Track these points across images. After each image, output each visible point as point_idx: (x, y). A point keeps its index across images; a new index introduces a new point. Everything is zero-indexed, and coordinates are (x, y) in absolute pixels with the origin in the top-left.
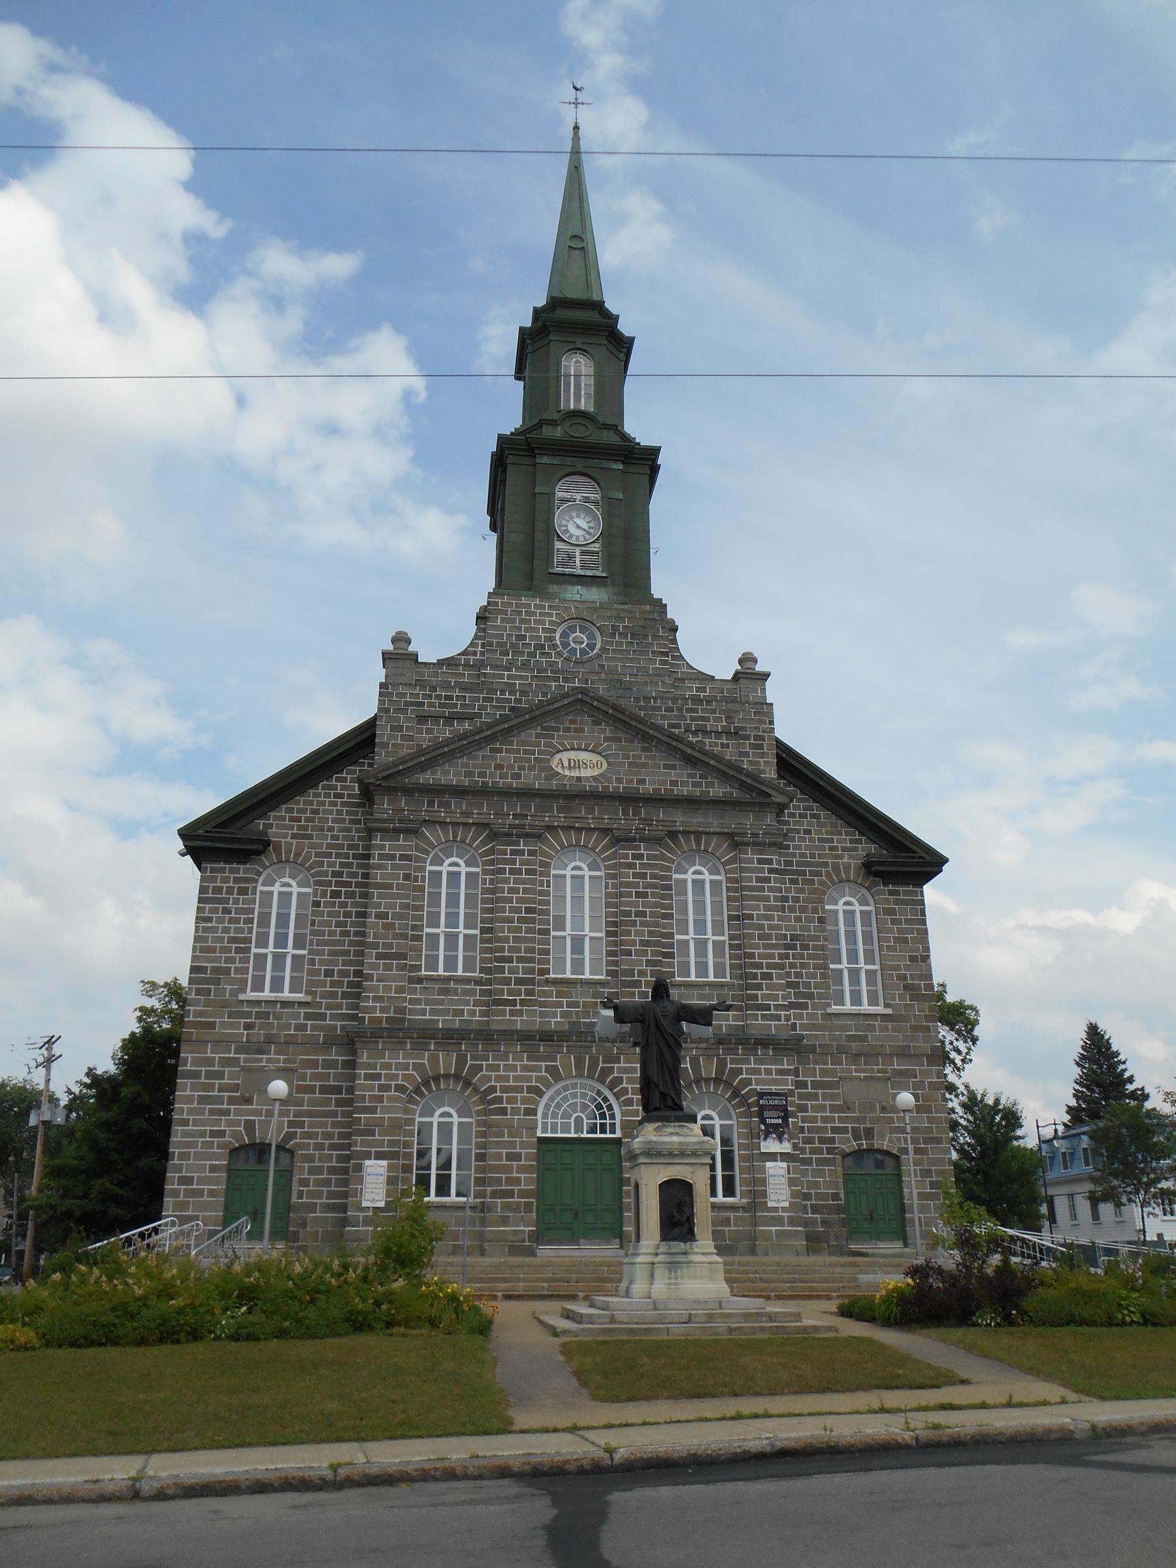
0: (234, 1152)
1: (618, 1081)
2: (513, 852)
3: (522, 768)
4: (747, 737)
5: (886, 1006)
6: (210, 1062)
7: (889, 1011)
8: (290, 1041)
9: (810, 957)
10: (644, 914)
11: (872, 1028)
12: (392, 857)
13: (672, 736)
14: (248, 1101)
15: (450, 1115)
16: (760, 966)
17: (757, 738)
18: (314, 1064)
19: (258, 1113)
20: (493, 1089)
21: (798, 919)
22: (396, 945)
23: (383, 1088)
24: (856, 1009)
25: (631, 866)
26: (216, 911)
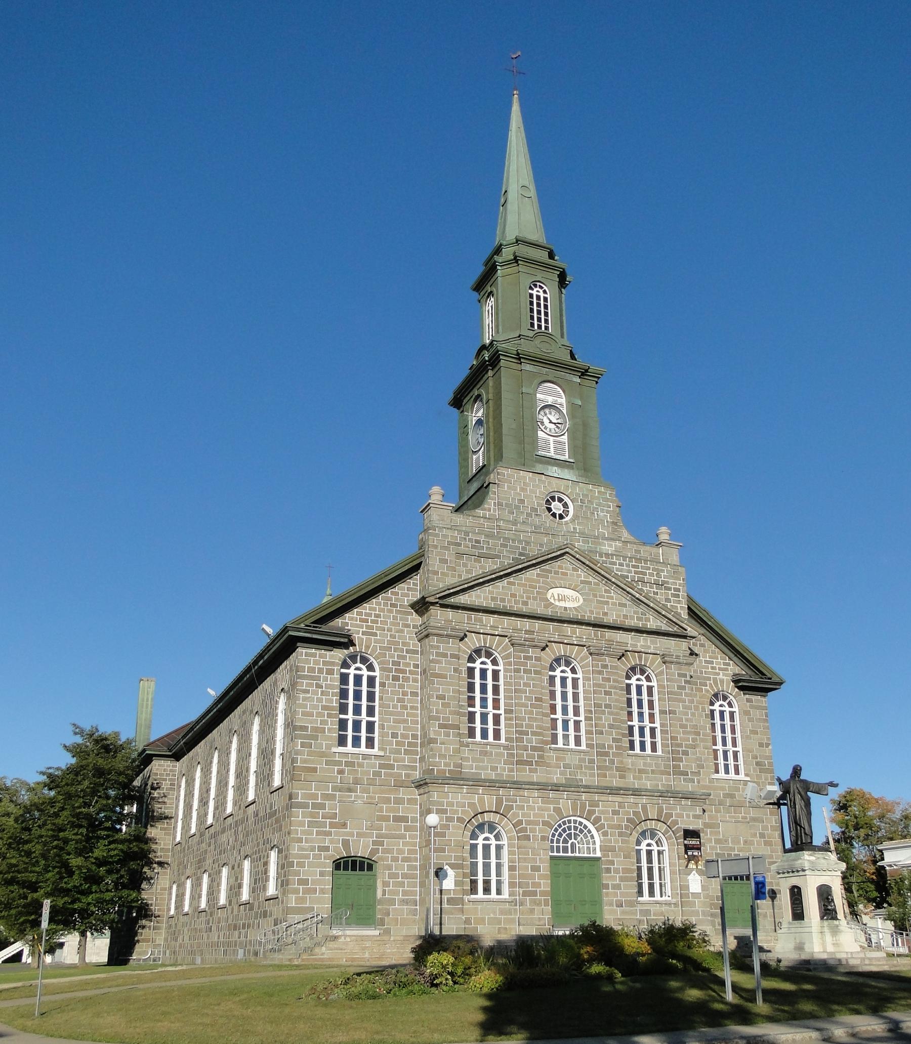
0: (337, 865)
4: (670, 589)
5: (746, 775)
6: (315, 796)
12: (445, 655)
14: (344, 825)
16: (680, 745)
17: (675, 590)
26: (311, 685)
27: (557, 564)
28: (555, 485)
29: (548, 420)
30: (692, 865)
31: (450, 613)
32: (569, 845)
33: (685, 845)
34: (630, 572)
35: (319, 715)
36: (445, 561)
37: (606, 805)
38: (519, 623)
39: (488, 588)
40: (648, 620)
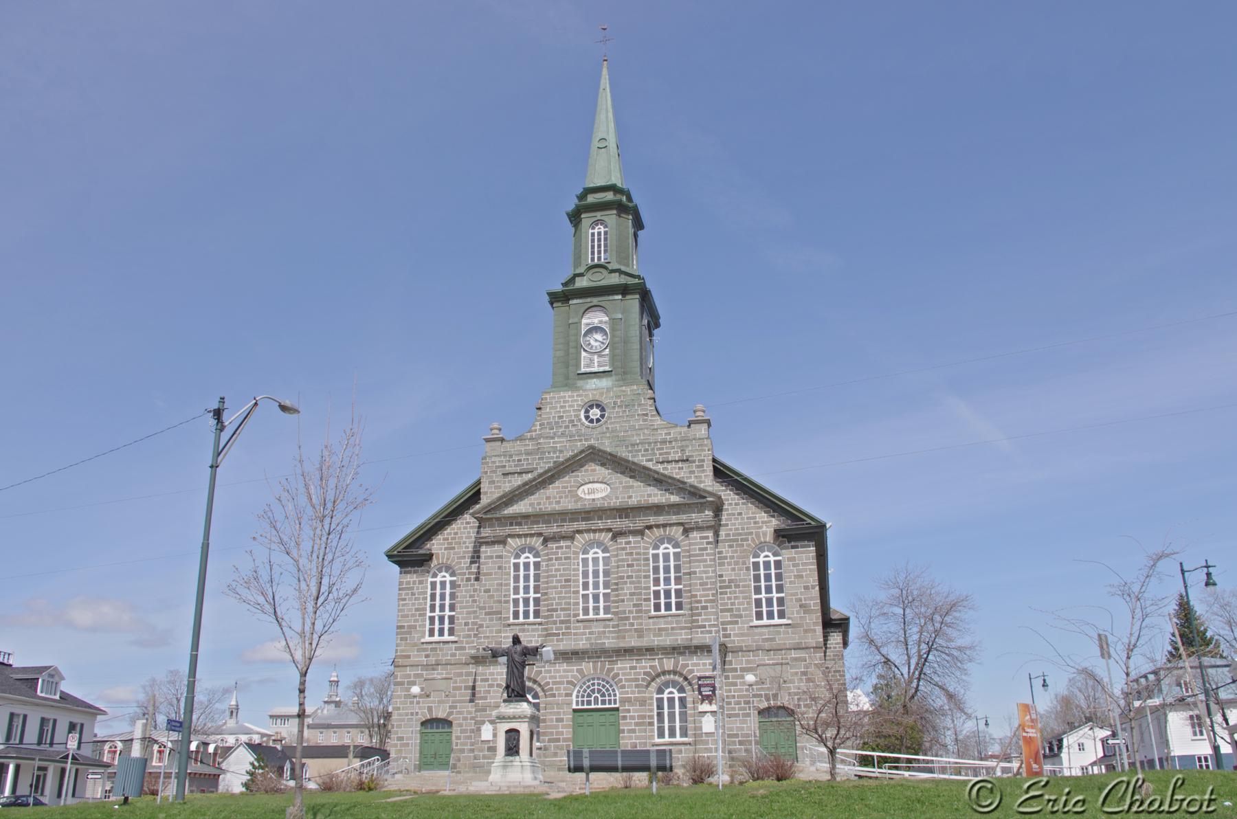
0: (423, 724)
1: (617, 675)
6: (409, 676)
9: (741, 592)
10: (631, 577)
11: (779, 633)
16: (700, 602)
18: (461, 674)
19: (434, 702)
20: (548, 683)
21: (733, 569)
22: (496, 607)
24: (442, 639)
25: (623, 549)
36: (493, 482)
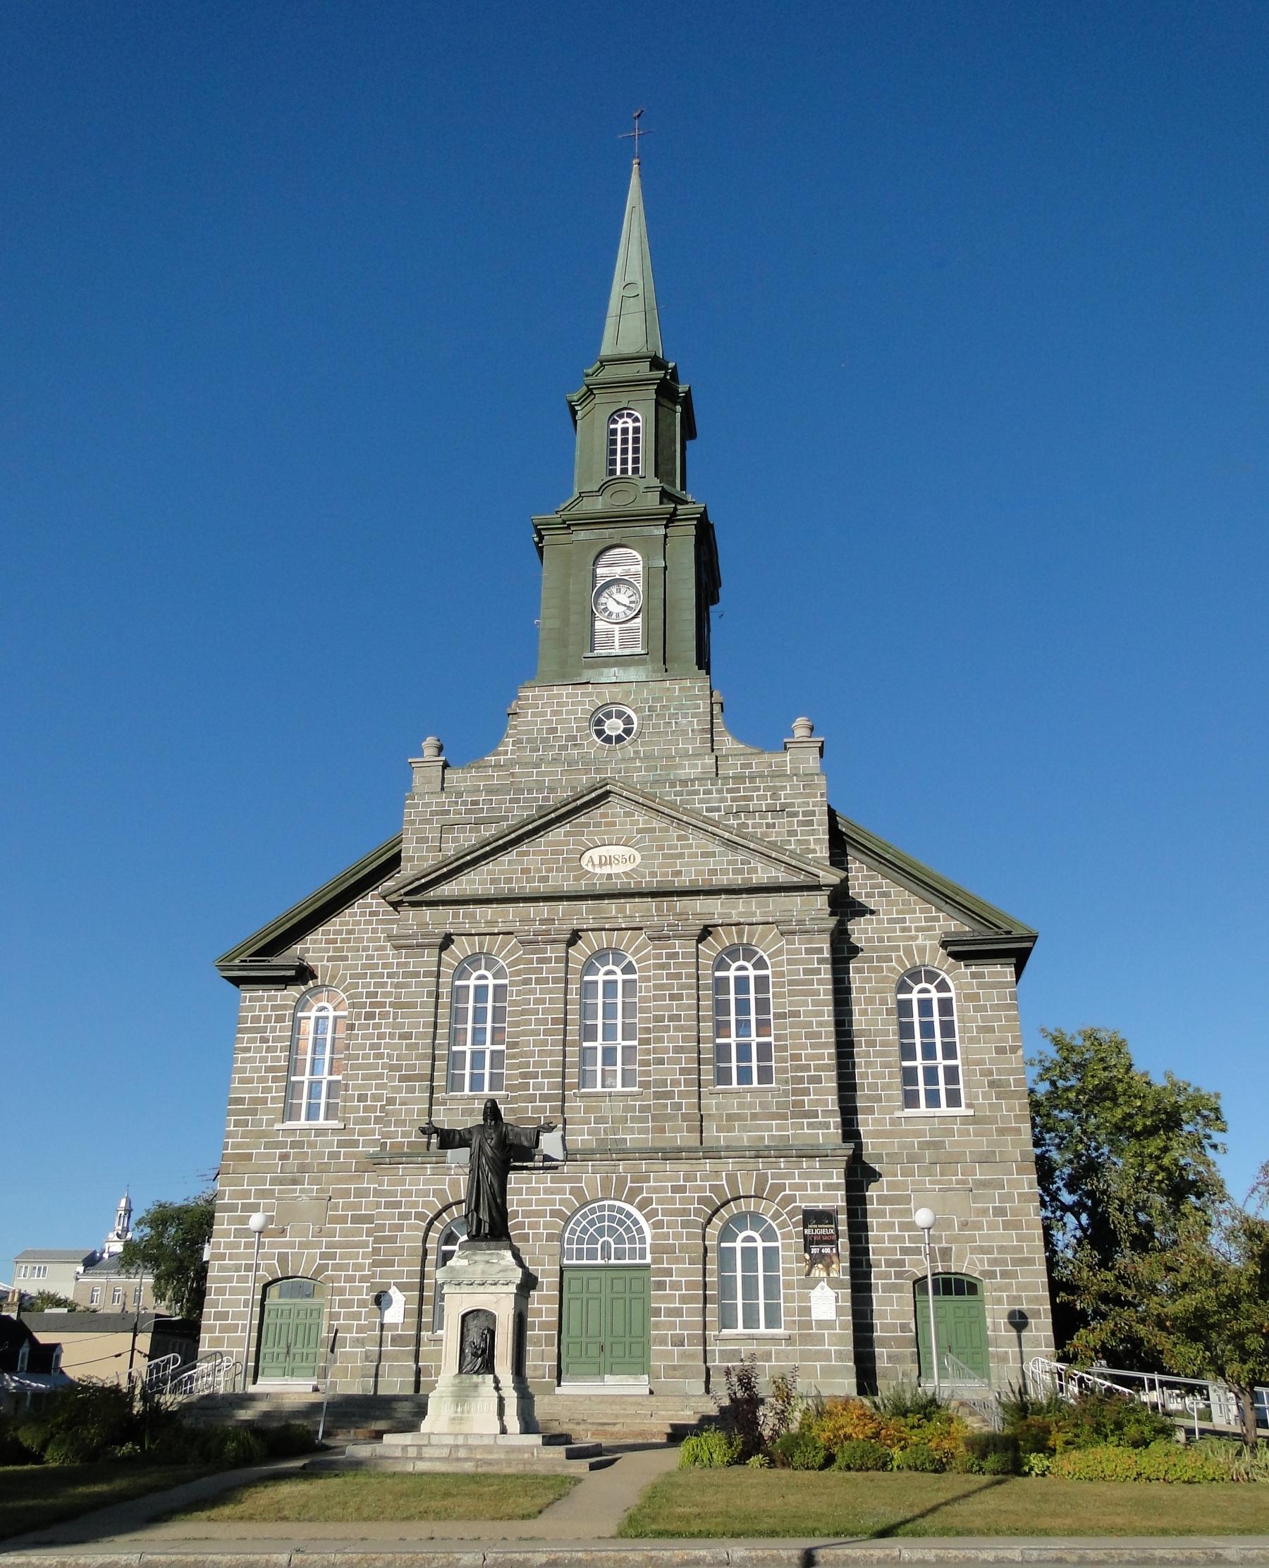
1: (648, 1201)
2: (540, 961)
3: (550, 870)
4: (795, 814)
5: (969, 1106)
6: (246, 1194)
7: (971, 1112)
8: (324, 1168)
12: (417, 975)
13: (708, 821)
15: (754, 1240)
16: (806, 1068)
23: (403, 1216)
27: (596, 813)
28: (607, 694)
29: (618, 603)
30: (819, 1271)
31: (427, 913)
32: (599, 1246)
33: (805, 1237)
34: (723, 800)
35: (262, 1080)
37: (662, 1179)
38: (531, 909)
39: (486, 869)
40: (755, 870)
